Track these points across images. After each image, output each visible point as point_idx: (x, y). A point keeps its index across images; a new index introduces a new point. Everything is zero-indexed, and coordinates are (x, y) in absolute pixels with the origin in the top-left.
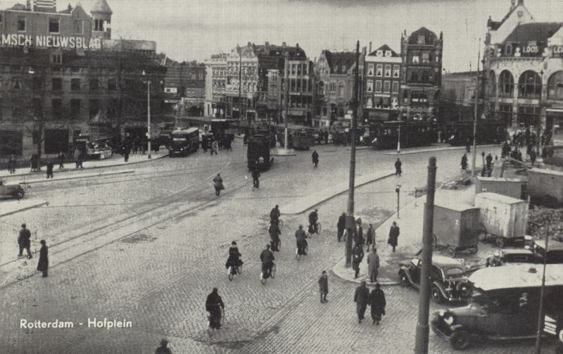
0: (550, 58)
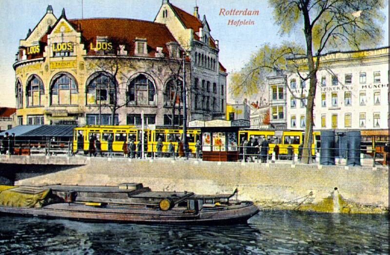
0: (50, 57)
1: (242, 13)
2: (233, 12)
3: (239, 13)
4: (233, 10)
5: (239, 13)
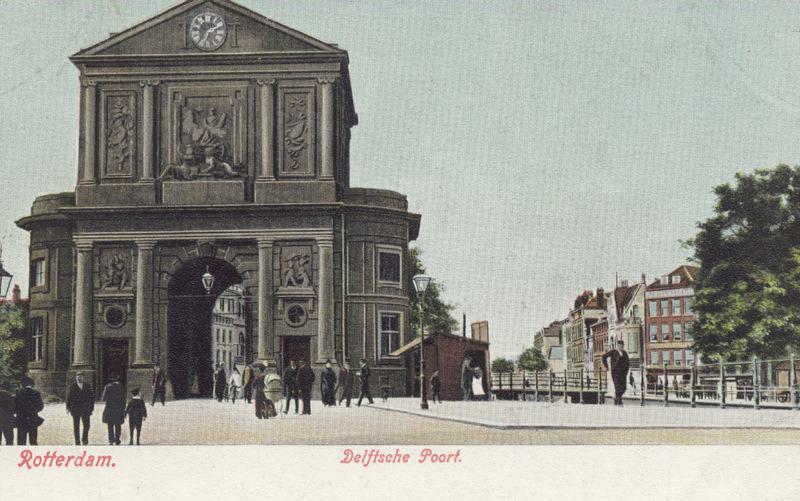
1: (72, 461)
2: (49, 460)
3: (64, 463)
4: (51, 454)
5: (64, 463)
